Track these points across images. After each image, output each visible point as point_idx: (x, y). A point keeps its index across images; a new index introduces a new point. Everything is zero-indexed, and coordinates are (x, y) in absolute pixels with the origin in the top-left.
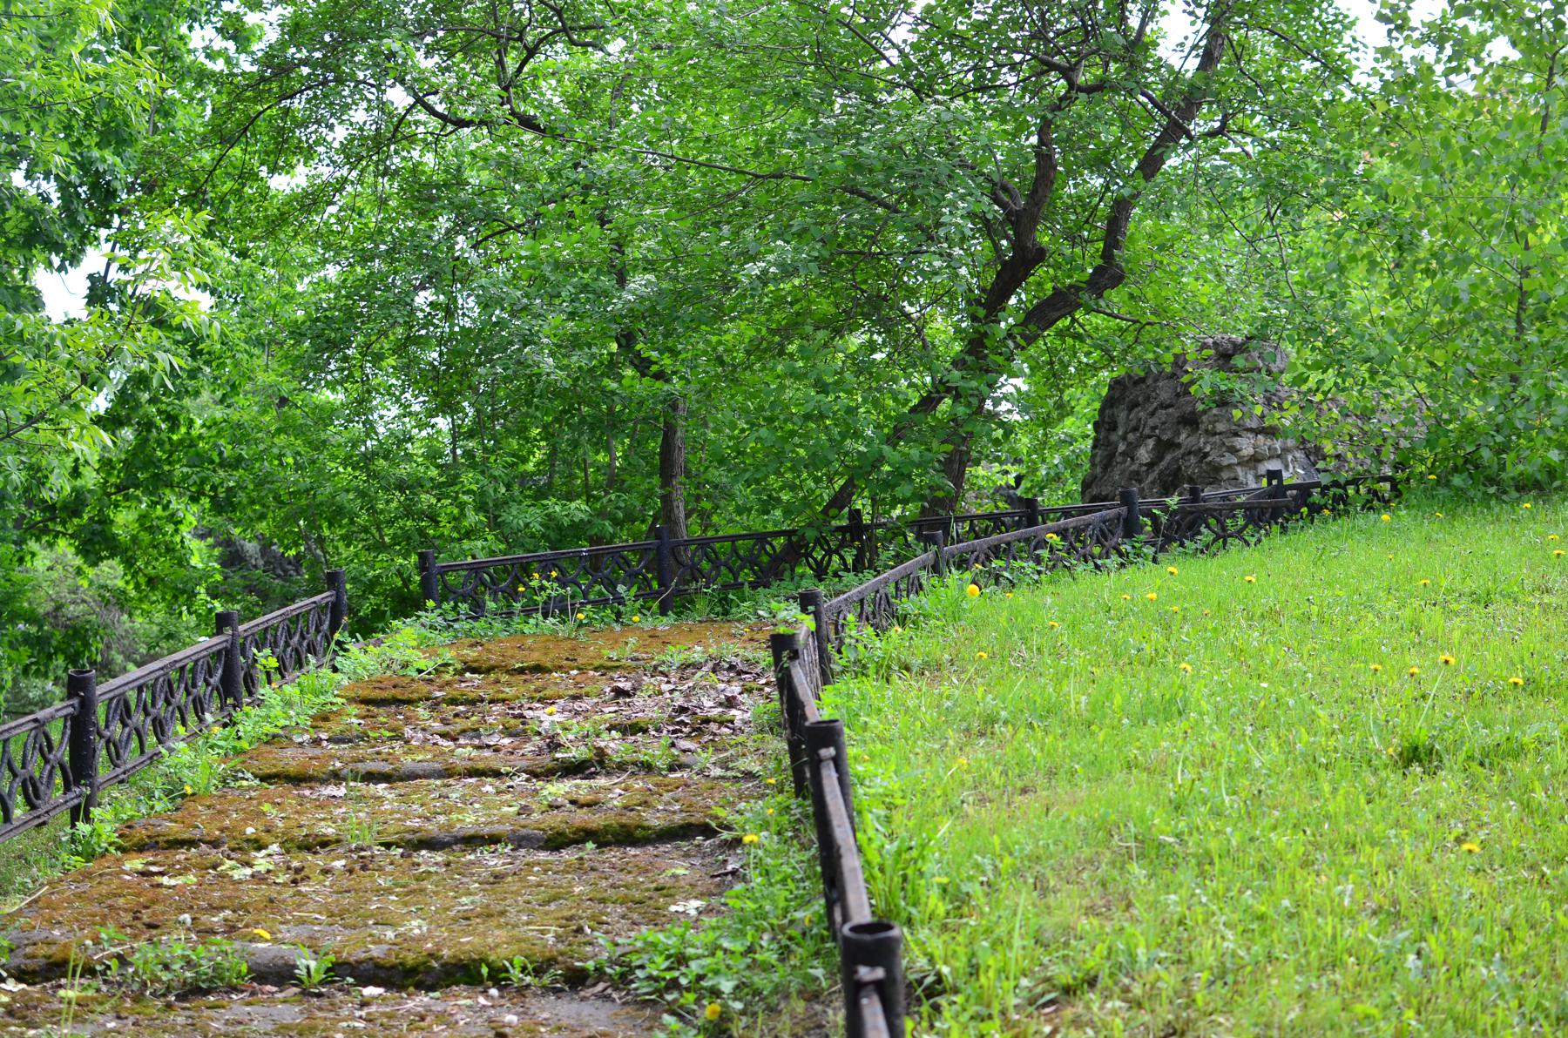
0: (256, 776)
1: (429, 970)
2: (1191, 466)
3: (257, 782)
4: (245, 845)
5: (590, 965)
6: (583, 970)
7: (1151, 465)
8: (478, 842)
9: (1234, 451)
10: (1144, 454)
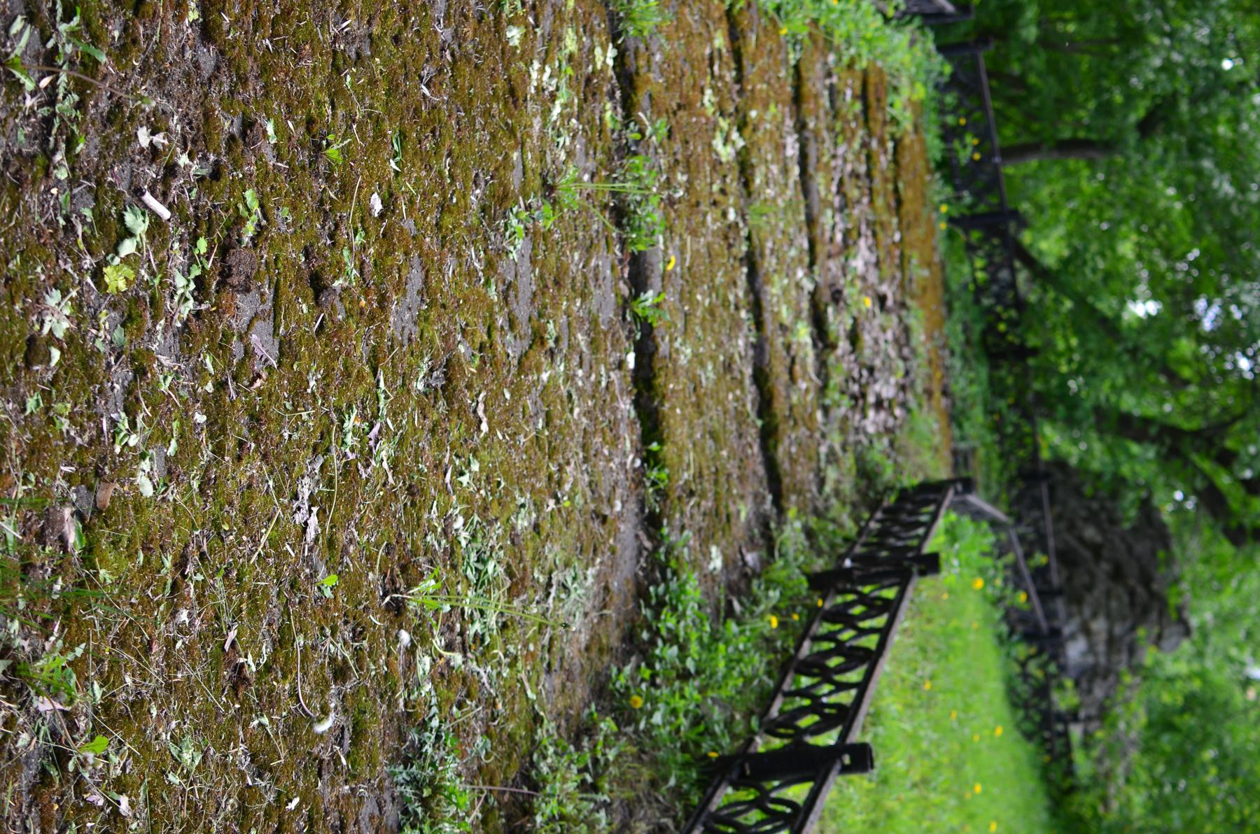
0: (798, 61)
1: (651, 399)
2: (1081, 578)
3: (793, 62)
4: (741, 115)
5: (665, 531)
6: (660, 526)
7: (1081, 539)
8: (761, 361)
9: (1095, 615)
10: (1090, 533)
